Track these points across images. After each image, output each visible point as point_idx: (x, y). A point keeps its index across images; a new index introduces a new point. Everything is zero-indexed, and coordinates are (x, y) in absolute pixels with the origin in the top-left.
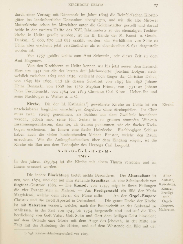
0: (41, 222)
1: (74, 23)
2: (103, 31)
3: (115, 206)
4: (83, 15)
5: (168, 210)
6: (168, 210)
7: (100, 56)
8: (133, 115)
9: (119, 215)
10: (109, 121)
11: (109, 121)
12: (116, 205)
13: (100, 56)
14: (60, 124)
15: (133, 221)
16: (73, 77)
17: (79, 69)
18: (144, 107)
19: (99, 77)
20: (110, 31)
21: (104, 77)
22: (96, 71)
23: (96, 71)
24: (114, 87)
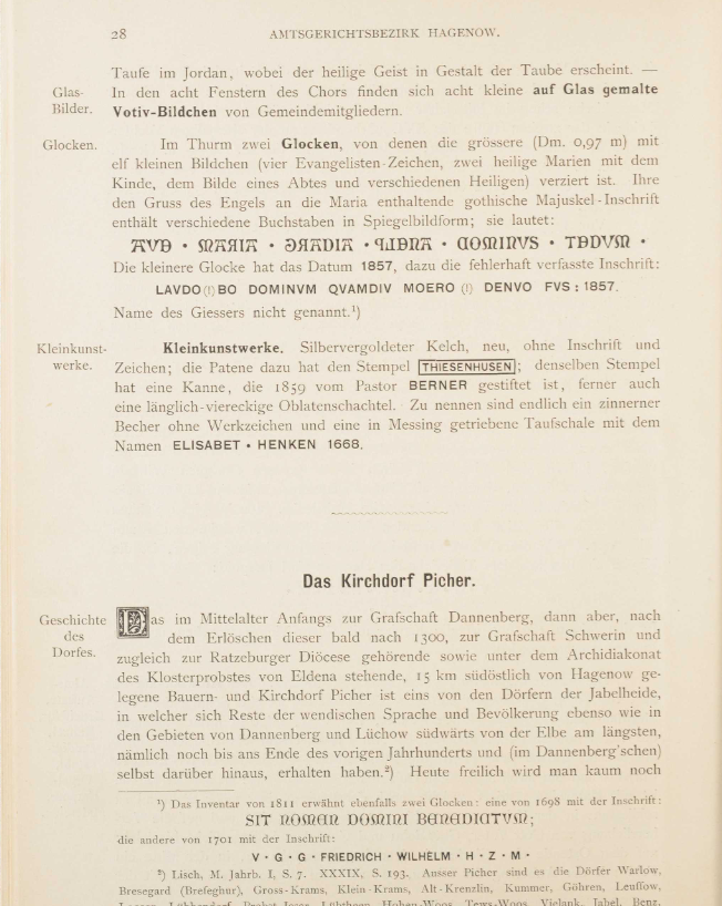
0: (386, 740)
1: (239, 668)
2: (460, 754)
3: (645, 200)
4: (299, 73)
5: (230, 408)
6: (230, 408)
7: (590, 637)
8: (242, 408)
9: (513, 159)
10: (475, 145)
11: (475, 145)
12: (649, 196)
13: (590, 637)
14: (295, 265)
15: (165, 314)
16: (298, 392)
17: (271, 86)
18: (290, 82)
19: (642, 771)
20: (348, 619)
21: (430, 92)
22: (414, 754)
23: (414, 754)
24: (226, 390)
